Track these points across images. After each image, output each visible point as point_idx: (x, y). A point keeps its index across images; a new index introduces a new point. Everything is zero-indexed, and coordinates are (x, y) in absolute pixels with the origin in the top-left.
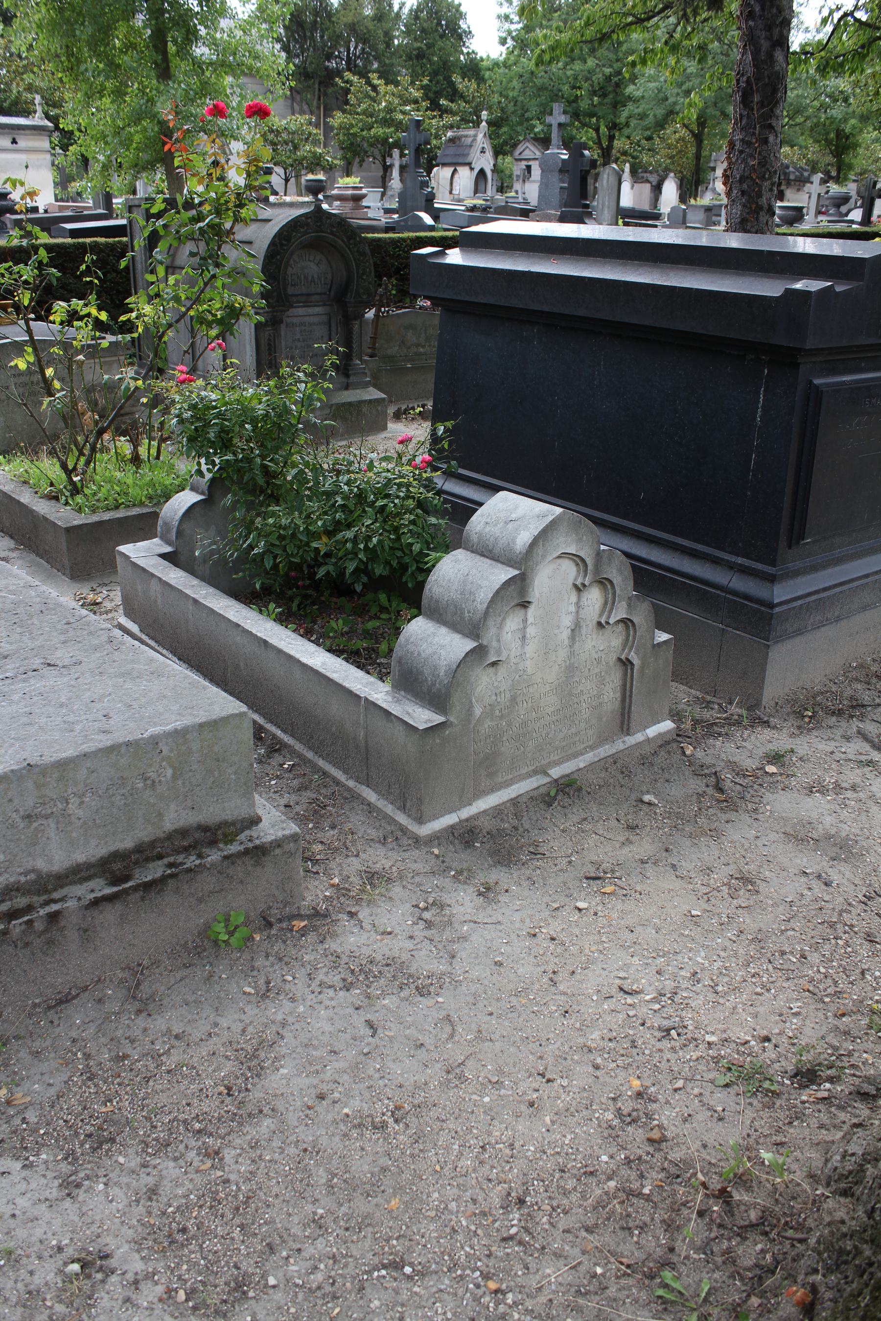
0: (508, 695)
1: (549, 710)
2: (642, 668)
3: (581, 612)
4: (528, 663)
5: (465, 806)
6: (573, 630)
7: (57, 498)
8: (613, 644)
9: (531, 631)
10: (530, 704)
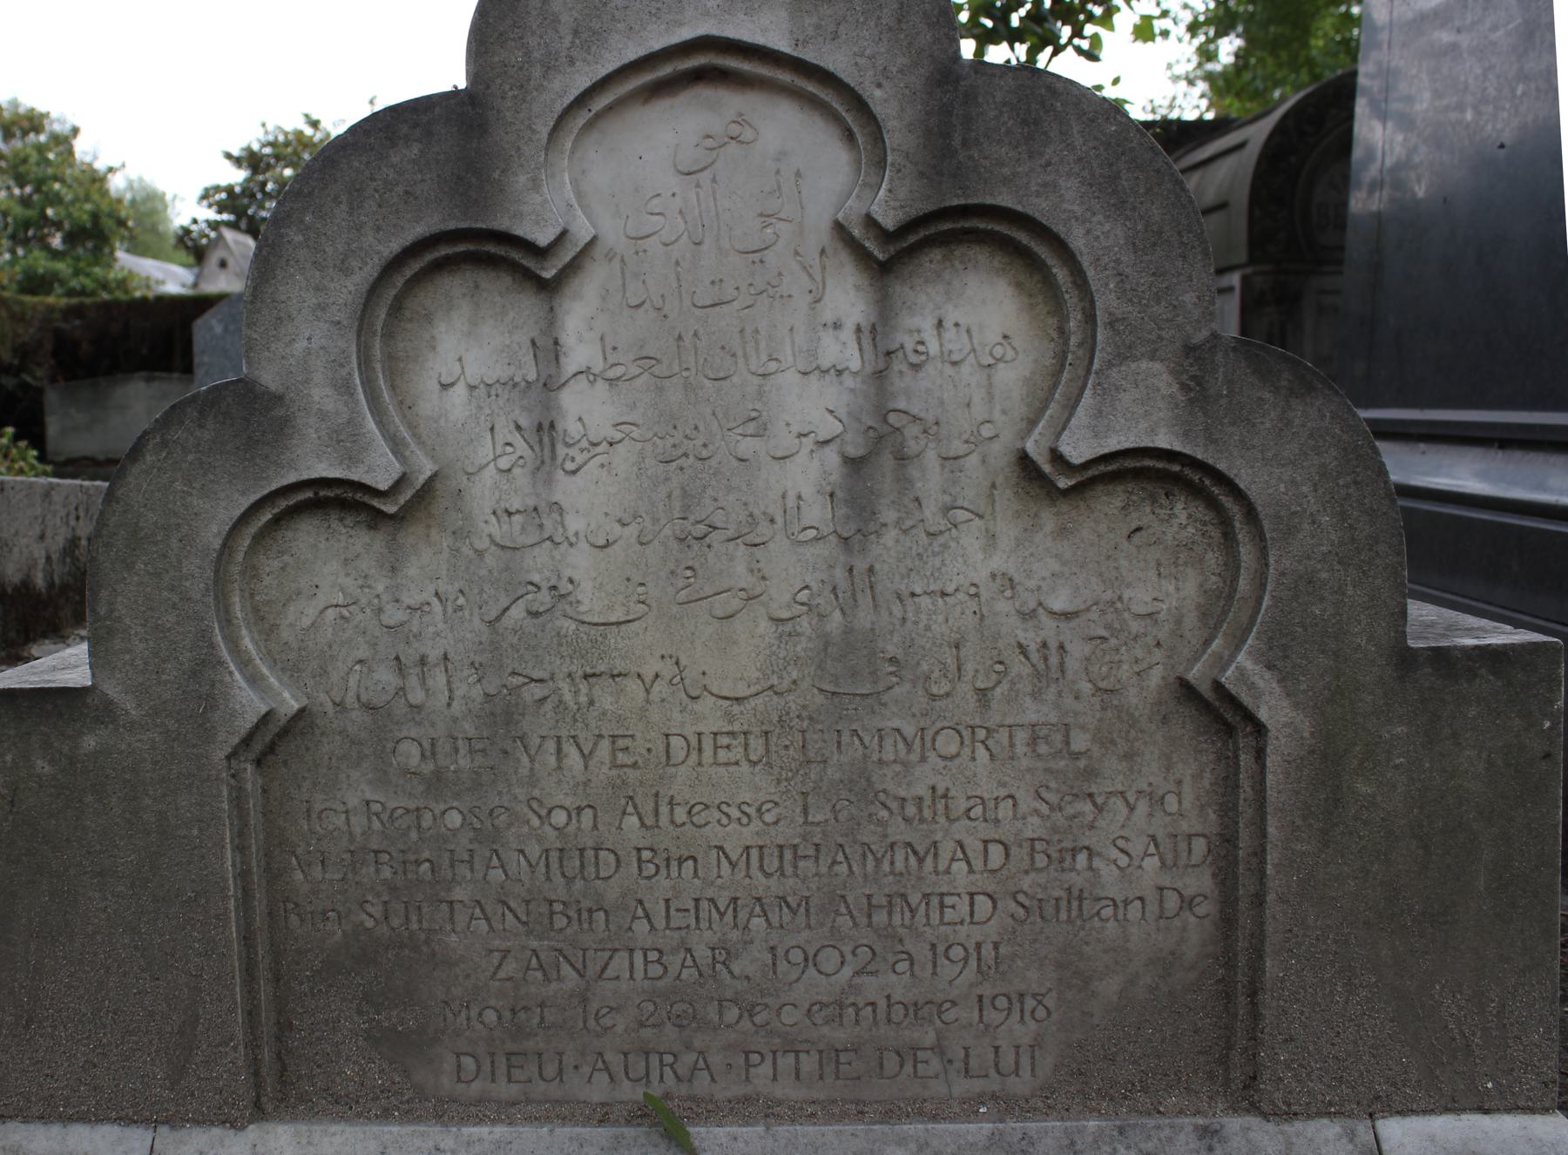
0: (469, 690)
1: (736, 837)
2: (1327, 759)
3: (902, 378)
4: (580, 562)
5: (201, 1121)
6: (854, 465)
7: (917, 499)
8: (1140, 597)
9: (585, 409)
10: (603, 773)
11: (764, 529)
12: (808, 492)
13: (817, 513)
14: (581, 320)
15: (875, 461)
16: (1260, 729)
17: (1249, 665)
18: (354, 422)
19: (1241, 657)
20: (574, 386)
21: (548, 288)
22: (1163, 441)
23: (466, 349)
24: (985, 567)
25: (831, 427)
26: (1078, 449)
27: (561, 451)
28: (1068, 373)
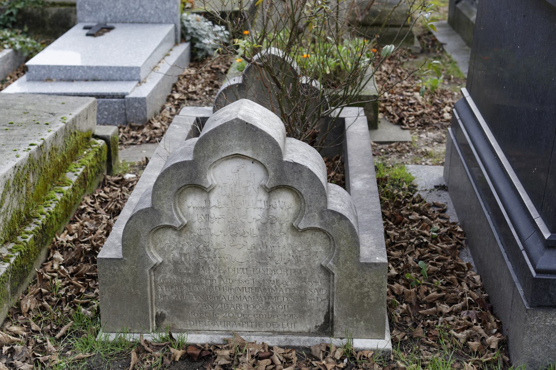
9: (215, 213)
11: (247, 234)
12: (255, 229)
13: (256, 232)
14: (214, 198)
15: (268, 222)
16: (333, 274)
17: (332, 264)
18: (173, 215)
19: (330, 262)
20: (214, 208)
21: (209, 192)
22: (316, 226)
23: (193, 202)
24: (285, 244)
25: (259, 217)
26: (302, 226)
27: (210, 219)
28: (300, 213)
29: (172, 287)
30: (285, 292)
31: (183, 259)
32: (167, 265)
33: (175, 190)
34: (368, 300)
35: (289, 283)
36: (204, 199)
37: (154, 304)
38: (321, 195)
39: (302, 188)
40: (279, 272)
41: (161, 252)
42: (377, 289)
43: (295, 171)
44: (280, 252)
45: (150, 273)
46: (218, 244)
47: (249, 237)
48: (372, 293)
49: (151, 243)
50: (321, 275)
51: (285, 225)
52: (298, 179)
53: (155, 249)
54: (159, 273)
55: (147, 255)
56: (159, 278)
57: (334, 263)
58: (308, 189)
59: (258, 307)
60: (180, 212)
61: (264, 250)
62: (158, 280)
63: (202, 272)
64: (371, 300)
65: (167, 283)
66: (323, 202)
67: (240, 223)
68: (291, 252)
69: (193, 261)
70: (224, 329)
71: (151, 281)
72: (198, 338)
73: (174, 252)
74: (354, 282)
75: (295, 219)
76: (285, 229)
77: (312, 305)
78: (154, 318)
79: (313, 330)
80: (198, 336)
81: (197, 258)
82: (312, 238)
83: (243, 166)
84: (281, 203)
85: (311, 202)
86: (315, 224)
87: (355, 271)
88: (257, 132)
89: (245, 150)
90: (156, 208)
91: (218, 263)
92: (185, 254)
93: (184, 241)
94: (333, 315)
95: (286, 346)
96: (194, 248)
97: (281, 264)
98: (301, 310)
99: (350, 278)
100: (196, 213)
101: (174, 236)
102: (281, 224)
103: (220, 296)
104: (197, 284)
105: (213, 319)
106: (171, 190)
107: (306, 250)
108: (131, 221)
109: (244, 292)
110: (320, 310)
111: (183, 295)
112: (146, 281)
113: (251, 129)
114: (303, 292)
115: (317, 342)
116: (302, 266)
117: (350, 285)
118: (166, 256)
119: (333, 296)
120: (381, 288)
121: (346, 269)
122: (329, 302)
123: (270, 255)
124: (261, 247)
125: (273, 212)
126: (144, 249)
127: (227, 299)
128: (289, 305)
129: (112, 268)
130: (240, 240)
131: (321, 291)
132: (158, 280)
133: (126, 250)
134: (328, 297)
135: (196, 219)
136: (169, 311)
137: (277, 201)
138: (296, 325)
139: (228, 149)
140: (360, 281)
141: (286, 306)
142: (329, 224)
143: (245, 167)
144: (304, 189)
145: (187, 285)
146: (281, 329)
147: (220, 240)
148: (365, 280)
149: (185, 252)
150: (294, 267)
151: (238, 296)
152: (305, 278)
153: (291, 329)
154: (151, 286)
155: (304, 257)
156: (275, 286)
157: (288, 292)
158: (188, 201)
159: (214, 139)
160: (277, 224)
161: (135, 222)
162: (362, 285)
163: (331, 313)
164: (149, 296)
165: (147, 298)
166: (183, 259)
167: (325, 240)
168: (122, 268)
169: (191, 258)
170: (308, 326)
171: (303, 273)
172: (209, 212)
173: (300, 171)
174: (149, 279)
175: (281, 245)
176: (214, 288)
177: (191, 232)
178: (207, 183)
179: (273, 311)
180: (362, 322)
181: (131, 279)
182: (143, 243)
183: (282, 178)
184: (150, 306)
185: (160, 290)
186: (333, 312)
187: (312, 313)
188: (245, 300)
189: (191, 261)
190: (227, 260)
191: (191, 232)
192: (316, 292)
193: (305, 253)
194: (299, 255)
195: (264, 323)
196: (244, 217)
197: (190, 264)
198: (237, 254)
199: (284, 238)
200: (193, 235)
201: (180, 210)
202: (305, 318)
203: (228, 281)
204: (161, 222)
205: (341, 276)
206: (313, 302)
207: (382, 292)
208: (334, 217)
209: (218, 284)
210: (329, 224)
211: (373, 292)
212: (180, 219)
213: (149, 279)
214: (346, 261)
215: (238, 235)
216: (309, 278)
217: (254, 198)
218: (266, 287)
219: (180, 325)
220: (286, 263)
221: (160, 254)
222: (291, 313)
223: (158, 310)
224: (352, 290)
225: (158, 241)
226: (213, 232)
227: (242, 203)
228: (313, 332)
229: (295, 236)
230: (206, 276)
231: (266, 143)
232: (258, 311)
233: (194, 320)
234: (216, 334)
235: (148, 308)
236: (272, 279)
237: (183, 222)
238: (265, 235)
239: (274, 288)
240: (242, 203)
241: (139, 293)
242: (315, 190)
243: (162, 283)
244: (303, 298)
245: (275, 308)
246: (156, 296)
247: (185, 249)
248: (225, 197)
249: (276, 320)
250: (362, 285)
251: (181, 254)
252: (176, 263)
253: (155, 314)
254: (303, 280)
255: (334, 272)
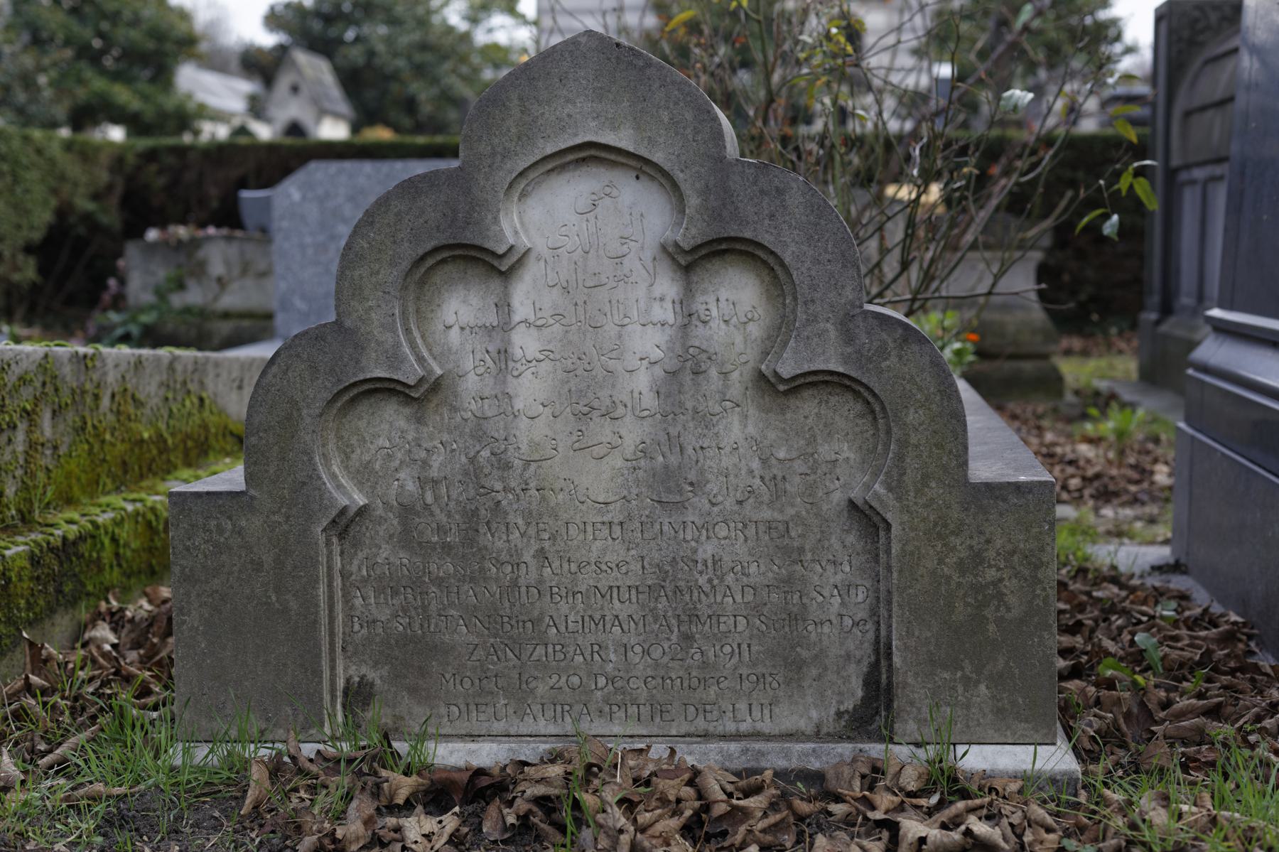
9: (525, 343)
11: (620, 411)
13: (649, 401)
14: (525, 295)
15: (686, 366)
16: (888, 526)
18: (398, 345)
19: (877, 486)
21: (506, 276)
23: (460, 308)
24: (739, 436)
25: (657, 354)
27: (511, 364)
29: (395, 593)
30: (738, 598)
31: (429, 498)
32: (381, 520)
33: (406, 265)
34: (997, 609)
35: (753, 569)
36: (492, 300)
37: (339, 650)
38: (844, 266)
39: (785, 245)
40: (722, 531)
41: (364, 476)
42: (1026, 572)
43: (762, 192)
44: (724, 464)
45: (328, 543)
46: (534, 445)
47: (629, 419)
48: (1010, 584)
49: (331, 446)
50: (851, 539)
51: (735, 376)
52: (772, 217)
53: (346, 467)
54: (357, 545)
55: (320, 478)
56: (356, 562)
57: (890, 489)
58: (805, 248)
59: (657, 653)
60: (419, 341)
61: (674, 460)
62: (354, 568)
63: (485, 539)
64: (1009, 609)
65: (380, 578)
66: (849, 289)
67: (599, 372)
68: (756, 464)
69: (458, 502)
70: (552, 729)
71: (330, 568)
72: (471, 752)
73: (402, 475)
74: (954, 549)
75: (766, 353)
76: (735, 391)
77: (826, 643)
78: (339, 694)
79: (830, 726)
80: (473, 746)
81: (472, 493)
82: (818, 415)
83: (608, 190)
84: (723, 304)
85: (813, 288)
86: (827, 361)
87: (955, 513)
88: (648, 72)
89: (614, 128)
90: (348, 323)
91: (534, 506)
92: (435, 482)
93: (431, 438)
94: (890, 666)
95: (746, 769)
96: (463, 459)
97: (727, 504)
98: (790, 663)
99: (940, 536)
100: (469, 347)
101: (402, 423)
102: (725, 374)
103: (540, 619)
104: (472, 579)
105: (521, 697)
106: (393, 264)
107: (804, 455)
108: (274, 369)
109: (616, 601)
110: (848, 657)
111: (428, 618)
112: (315, 564)
113: (630, 63)
114: (796, 597)
115: (841, 755)
116: (792, 511)
117: (941, 562)
118: (379, 491)
119: (889, 603)
120: (1037, 567)
121: (926, 506)
122: (878, 630)
123: (692, 476)
124: (666, 449)
125: (699, 334)
126: (311, 459)
127: (563, 629)
128: (754, 642)
129: (213, 523)
130: (602, 431)
131: (853, 591)
132: (354, 568)
133: (255, 463)
134: (874, 612)
135: (468, 364)
136: (385, 671)
137: (711, 299)
138: (776, 710)
139: (563, 129)
140: (971, 547)
141: (744, 646)
142: (869, 360)
143: (615, 193)
144: (793, 248)
145: (439, 582)
146: (731, 727)
147: (540, 430)
148: (988, 542)
149: (434, 473)
150: (767, 514)
151: (597, 617)
152: (801, 550)
153: (759, 726)
154: (330, 585)
155: (797, 479)
156: (710, 581)
157: (749, 598)
158: (444, 307)
159: (521, 99)
160: (713, 372)
161: (285, 372)
162: (978, 558)
163: (883, 663)
164: (324, 620)
165: (315, 622)
166: (429, 498)
167: (860, 422)
168: (243, 523)
169: (454, 494)
170: (814, 714)
171: (793, 534)
172: (509, 342)
173: (777, 189)
174: (323, 559)
175: (727, 443)
176: (523, 589)
177: (454, 409)
178: (500, 236)
179: (705, 665)
180: (982, 687)
181: (268, 559)
182: (308, 438)
183: (725, 213)
184: (325, 648)
185: (358, 602)
186: (889, 655)
187: (826, 669)
188: (617, 630)
189: (452, 504)
190: (560, 497)
191: (454, 409)
192: (837, 593)
193: (799, 466)
194: (780, 476)
195: (676, 704)
196: (614, 355)
197: (449, 515)
198: (596, 477)
199: (735, 420)
200: (458, 419)
201: (423, 337)
202: (805, 684)
203: (566, 566)
204: (362, 370)
205: (912, 529)
206: (826, 629)
207: (1040, 582)
208: (884, 336)
209: (533, 576)
210: (869, 360)
211: (1014, 581)
212: (421, 360)
213: (323, 559)
214: (926, 478)
215: (595, 414)
216: (813, 551)
217: (641, 292)
218: (682, 584)
219: (415, 714)
220: (740, 503)
221: (360, 485)
222: (760, 669)
223: (353, 670)
224: (949, 578)
225: (354, 441)
226: (519, 404)
227: (607, 309)
228: (828, 734)
229: (768, 411)
230: (499, 551)
231: (676, 104)
232: (657, 664)
233: (460, 701)
234: (529, 742)
235: (319, 656)
236: (700, 556)
237: (431, 372)
238: (678, 411)
239: (707, 588)
240: (607, 309)
241: (293, 605)
242: (826, 251)
243: (365, 581)
244: (796, 618)
245: (711, 654)
246: (345, 625)
247: (436, 465)
248: (556, 292)
249: (712, 696)
250: (978, 558)
251: (422, 482)
252: (407, 511)
253: (341, 683)
254: (795, 556)
255: (889, 516)
